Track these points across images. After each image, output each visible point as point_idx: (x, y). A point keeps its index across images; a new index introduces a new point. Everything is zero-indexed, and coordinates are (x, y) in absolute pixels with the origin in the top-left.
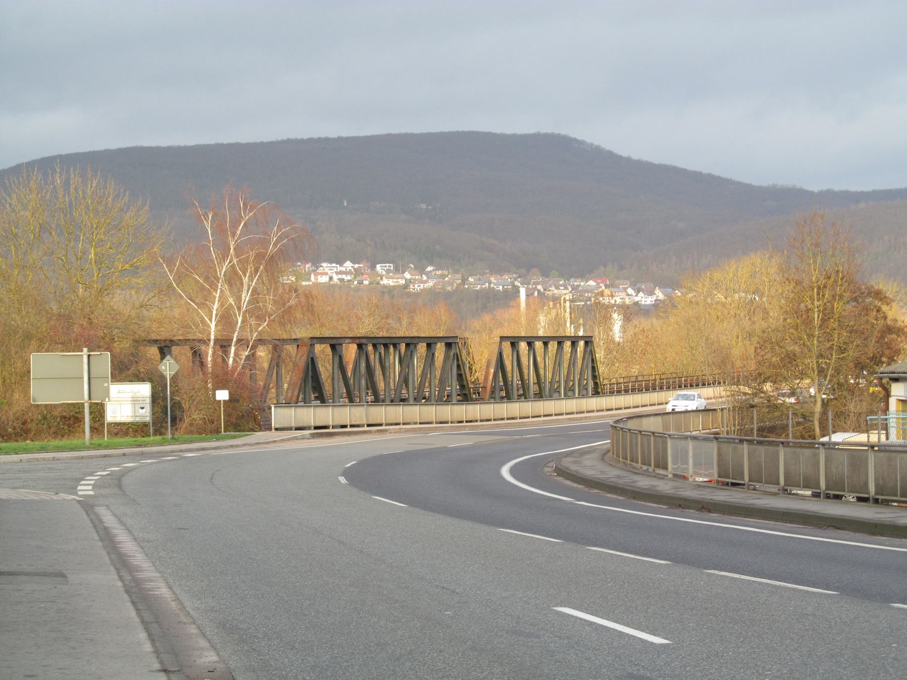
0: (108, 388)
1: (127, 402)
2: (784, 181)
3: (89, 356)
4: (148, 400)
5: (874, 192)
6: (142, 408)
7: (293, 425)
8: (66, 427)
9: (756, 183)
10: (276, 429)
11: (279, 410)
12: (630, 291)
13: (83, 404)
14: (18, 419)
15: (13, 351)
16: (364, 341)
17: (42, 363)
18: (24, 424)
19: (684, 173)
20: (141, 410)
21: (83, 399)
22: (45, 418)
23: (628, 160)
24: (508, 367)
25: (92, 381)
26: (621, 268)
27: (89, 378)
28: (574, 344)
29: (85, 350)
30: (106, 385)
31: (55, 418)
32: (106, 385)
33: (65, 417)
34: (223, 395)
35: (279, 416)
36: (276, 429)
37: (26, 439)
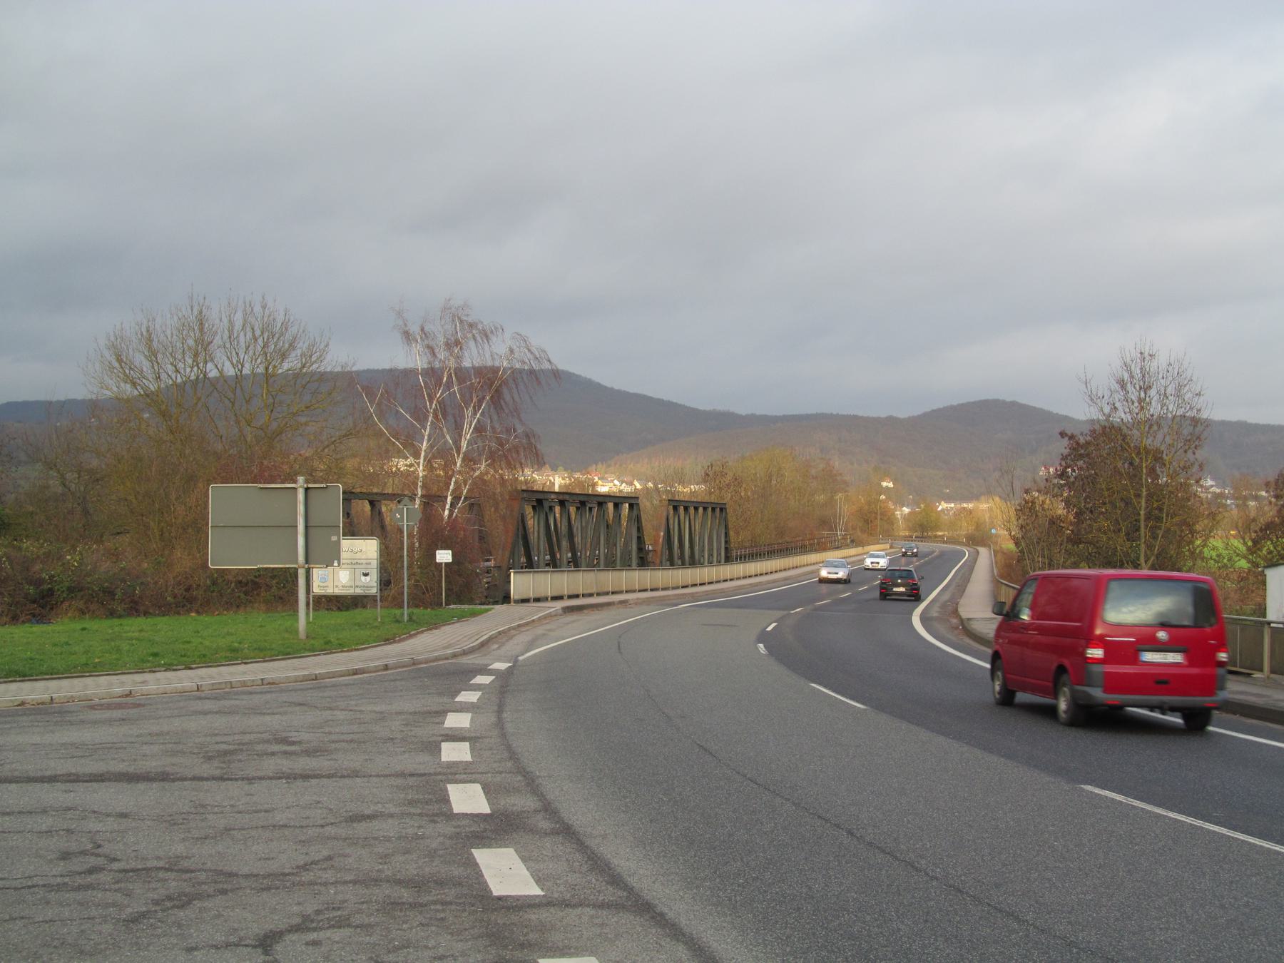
0: (338, 542)
1: (353, 566)
2: (721, 407)
3: (307, 489)
4: (375, 563)
5: (784, 416)
6: (366, 575)
7: (531, 596)
8: (242, 596)
9: (701, 408)
10: (517, 602)
11: (519, 577)
12: (616, 482)
13: (296, 570)
14: (179, 583)
15: (173, 496)
16: (567, 497)
17: (224, 502)
18: (188, 590)
19: (650, 398)
20: (363, 578)
21: (296, 562)
22: (214, 583)
23: (612, 389)
24: (533, 538)
25: (311, 531)
26: (609, 466)
27: (307, 527)
28: (696, 509)
29: (301, 479)
30: (334, 538)
31: (229, 582)
32: (334, 538)
33: (240, 582)
34: (444, 556)
35: (520, 583)
36: (517, 602)
37: (190, 611)
